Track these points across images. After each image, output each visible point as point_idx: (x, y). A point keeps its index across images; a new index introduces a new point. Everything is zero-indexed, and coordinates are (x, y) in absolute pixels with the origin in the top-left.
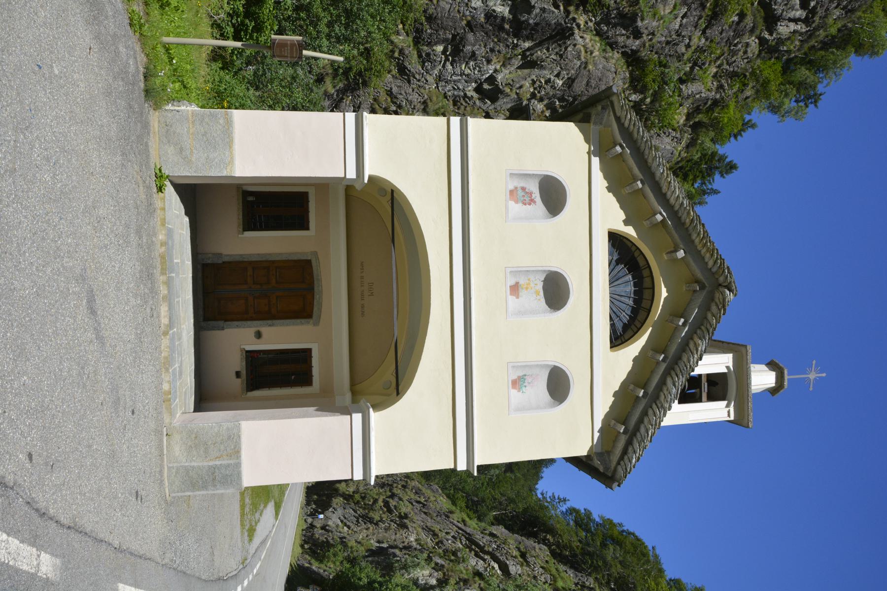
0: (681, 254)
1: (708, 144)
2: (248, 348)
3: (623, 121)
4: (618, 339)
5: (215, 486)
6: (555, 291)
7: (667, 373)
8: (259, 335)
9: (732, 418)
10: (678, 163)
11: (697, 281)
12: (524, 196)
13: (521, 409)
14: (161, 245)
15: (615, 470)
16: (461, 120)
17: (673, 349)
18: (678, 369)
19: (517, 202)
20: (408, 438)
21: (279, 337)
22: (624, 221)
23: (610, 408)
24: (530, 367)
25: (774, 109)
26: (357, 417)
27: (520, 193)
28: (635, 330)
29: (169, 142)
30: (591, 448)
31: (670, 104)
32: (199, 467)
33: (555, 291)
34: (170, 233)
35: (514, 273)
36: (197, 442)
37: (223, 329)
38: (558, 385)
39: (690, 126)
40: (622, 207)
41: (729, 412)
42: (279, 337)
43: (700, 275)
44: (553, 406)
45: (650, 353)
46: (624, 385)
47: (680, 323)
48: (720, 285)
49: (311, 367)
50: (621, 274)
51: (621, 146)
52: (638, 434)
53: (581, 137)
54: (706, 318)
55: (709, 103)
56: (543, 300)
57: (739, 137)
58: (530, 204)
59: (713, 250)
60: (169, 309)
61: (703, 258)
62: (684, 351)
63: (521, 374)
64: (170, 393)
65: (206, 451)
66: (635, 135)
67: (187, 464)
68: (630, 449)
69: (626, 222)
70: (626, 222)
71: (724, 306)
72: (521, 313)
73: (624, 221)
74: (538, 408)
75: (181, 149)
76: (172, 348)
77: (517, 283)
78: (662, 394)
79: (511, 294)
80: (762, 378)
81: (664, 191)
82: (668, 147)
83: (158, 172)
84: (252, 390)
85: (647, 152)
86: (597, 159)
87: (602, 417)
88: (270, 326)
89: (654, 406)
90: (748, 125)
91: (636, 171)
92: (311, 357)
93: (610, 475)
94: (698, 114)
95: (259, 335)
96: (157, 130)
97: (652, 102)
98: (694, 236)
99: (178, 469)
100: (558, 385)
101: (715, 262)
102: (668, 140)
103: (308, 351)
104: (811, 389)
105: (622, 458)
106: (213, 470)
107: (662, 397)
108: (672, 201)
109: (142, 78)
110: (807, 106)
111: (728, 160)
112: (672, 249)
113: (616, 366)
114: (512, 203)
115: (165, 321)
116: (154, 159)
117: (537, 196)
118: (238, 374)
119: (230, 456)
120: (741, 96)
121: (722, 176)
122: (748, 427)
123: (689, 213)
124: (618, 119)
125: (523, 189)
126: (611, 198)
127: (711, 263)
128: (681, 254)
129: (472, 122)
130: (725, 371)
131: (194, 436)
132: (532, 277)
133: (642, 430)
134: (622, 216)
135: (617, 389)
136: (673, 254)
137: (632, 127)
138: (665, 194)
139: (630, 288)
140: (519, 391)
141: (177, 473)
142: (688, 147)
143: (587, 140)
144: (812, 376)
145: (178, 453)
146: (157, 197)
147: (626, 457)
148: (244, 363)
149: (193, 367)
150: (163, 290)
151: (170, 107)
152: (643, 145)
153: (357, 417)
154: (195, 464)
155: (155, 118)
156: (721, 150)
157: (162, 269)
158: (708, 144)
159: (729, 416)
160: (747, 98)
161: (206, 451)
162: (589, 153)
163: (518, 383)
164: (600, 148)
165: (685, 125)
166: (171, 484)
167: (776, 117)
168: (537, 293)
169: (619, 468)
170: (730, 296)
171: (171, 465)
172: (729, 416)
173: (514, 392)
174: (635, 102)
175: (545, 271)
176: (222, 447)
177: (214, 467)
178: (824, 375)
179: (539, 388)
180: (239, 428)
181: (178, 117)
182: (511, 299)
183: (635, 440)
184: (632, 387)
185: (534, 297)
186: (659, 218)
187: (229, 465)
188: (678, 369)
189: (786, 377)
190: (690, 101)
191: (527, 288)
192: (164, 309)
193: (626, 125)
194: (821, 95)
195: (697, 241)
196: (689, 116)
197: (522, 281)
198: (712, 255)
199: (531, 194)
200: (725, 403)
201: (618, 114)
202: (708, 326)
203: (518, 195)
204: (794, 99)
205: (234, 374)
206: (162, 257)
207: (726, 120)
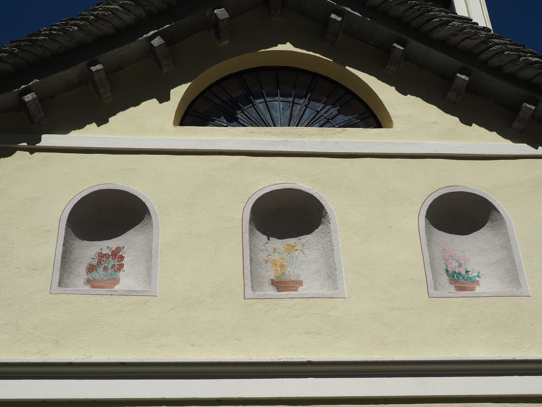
0: (221, 13)
4: (370, 115)
7: (425, 38)
12: (105, 269)
13: (513, 275)
19: (116, 281)
22: (161, 102)
23: (491, 130)
24: (432, 260)
27: (100, 274)
33: (288, 215)
35: (255, 284)
46: (448, 108)
47: (339, 19)
50: (255, 114)
56: (304, 239)
58: (122, 258)
63: (445, 279)
69: (164, 98)
70: (164, 98)
72: (332, 274)
73: (161, 102)
74: (507, 246)
86: (44, 137)
87: (508, 143)
89: (484, 56)
91: (72, 73)
108: (128, 18)
117: (106, 246)
125: (91, 269)
126: (117, 120)
128: (221, 13)
132: (262, 256)
133: (529, 73)
135: (457, 119)
140: (477, 283)
162: (32, 151)
163: (461, 281)
173: (478, 290)
175: (251, 230)
179: (471, 249)
184: (451, 95)
185: (300, 254)
186: (157, 42)
191: (282, 266)
197: (271, 273)
199: (101, 256)
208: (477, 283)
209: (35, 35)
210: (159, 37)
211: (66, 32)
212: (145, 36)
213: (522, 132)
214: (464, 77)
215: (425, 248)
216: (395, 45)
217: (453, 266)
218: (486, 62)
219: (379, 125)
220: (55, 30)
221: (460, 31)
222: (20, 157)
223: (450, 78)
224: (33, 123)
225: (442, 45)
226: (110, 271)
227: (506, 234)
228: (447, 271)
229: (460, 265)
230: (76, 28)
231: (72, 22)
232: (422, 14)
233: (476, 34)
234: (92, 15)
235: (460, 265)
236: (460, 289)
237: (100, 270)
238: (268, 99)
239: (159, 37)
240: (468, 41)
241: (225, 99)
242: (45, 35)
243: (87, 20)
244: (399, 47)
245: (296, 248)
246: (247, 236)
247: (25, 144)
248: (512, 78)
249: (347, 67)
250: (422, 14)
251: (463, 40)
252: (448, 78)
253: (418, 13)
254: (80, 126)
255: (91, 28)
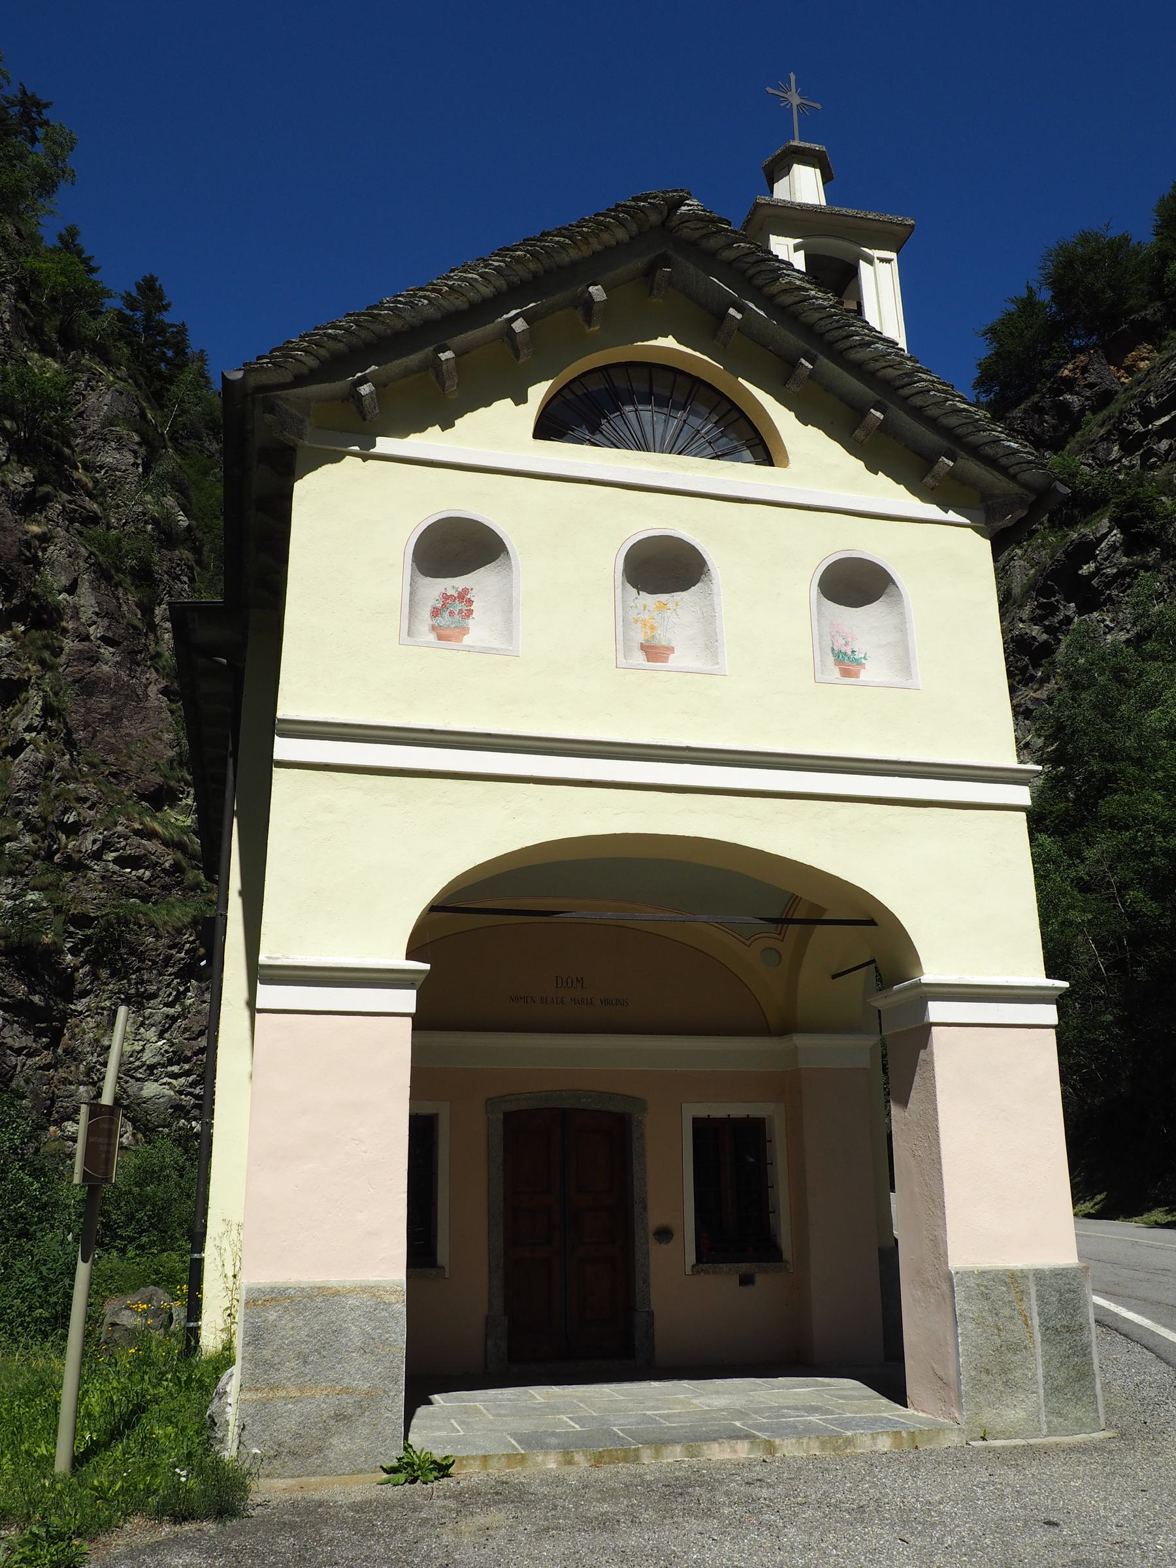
1: (103, 323)
2: (691, 1258)
3: (305, 371)
4: (762, 449)
5: (1081, 1327)
6: (665, 567)
7: (839, 357)
8: (664, 1234)
9: (892, 255)
10: (137, 385)
11: (649, 272)
12: (451, 614)
13: (904, 661)
14: (570, 1462)
15: (1025, 485)
16: (283, 735)
17: (790, 339)
18: (835, 333)
19: (465, 630)
20: (969, 901)
21: (669, 1190)
23: (898, 481)
25: (47, 184)
26: (937, 1011)
27: (444, 620)
28: (734, 415)
29: (320, 1450)
30: (976, 530)
31: (21, 383)
32: (1047, 1363)
33: (665, 567)
34: (535, 1442)
36: (1000, 1371)
37: (651, 1314)
38: (855, 583)
39: (67, 352)
40: (488, 404)
41: (882, 260)
42: (669, 1190)
43: (638, 264)
44: (898, 597)
45: (792, 387)
46: (854, 449)
47: (739, 316)
48: (663, 224)
49: (729, 1120)
51: (362, 381)
52: (960, 431)
53: (327, 471)
54: (730, 263)
55: (24, 306)
56: (678, 596)
57: (93, 264)
58: (470, 602)
59: (599, 223)
60: (715, 1440)
61: (608, 248)
62: (795, 317)
64: (897, 1434)
65: (1014, 1348)
66: (341, 346)
67: (1041, 1392)
68: (988, 450)
69: (520, 399)
70: (520, 399)
71: (713, 221)
72: (710, 643)
74: (902, 628)
75: (340, 1417)
76: (802, 1432)
77: (644, 647)
78: (881, 373)
79: (665, 660)
80: (804, 186)
81: (466, 306)
82: (108, 398)
83: (401, 1477)
84: (779, 1252)
85: (378, 328)
86: (379, 439)
87: (916, 501)
88: (645, 1208)
89: (906, 391)
90: (69, 241)
91: (414, 359)
92: (708, 1120)
93: (1033, 498)
94: (43, 332)
95: (664, 1234)
96: (291, 1482)
97: (12, 417)
98: (564, 258)
99: (1052, 1412)
100: (855, 583)
101: (622, 223)
102: (92, 399)
103: (702, 1127)
104: (818, 106)
105: (1003, 470)
106: (1051, 1333)
107: (890, 372)
108: (486, 291)
109: (188, 1528)
110: (46, 123)
111: (134, 293)
112: (579, 313)
113: (815, 459)
114: (467, 640)
115: (742, 1451)
116: (365, 1487)
118: (746, 1280)
119: (1023, 1294)
120: (15, 243)
121: (166, 308)
122: (912, 227)
123: (518, 260)
124: (300, 380)
125: (436, 613)
127: (621, 234)
129: (286, 709)
130: (802, 253)
131: (984, 1376)
132: (632, 614)
133: (953, 421)
134: (504, 406)
136: (596, 308)
137: (322, 352)
138: (472, 305)
139: (648, 416)
141: (1060, 1414)
142: (107, 362)
143: (337, 458)
144: (795, 100)
145: (1019, 1414)
146: (468, 1475)
147: (1004, 461)
148: (724, 1267)
149: (685, 1384)
150: (675, 1454)
151: (229, 1452)
152: (364, 334)
153: (937, 1011)
154: (1040, 1372)
155: (270, 1489)
156: (113, 304)
157: (625, 1460)
158: (103, 323)
159: (889, 261)
160: (19, 233)
161: (1014, 1348)
162: (365, 458)
163: (847, 664)
164: (354, 430)
165: (64, 362)
166: (1081, 1426)
167: (63, 186)
168: (663, 607)
169: (1023, 477)
170: (692, 205)
171: (1045, 1427)
172: (889, 261)
173: (864, 675)
174: (10, 450)
176: (1006, 1312)
177: (1046, 1329)
178: (793, 77)
180: (966, 1274)
181: (258, 1428)
182: (674, 660)
183: (971, 438)
186: (519, 326)
187: (1041, 1297)
188: (835, 333)
189: (796, 143)
190: (17, 344)
191: (652, 628)
192: (718, 1453)
193: (311, 362)
194: (24, 93)
195: (574, 254)
196: (47, 350)
197: (640, 636)
198: (607, 227)
200: (863, 266)
201: (289, 378)
202: (751, 259)
203: (450, 620)
204: (29, 147)
205: (748, 1289)
206: (598, 1461)
207: (61, 279)
208: (862, 665)
209: (375, 307)
210: (521, 319)
211: (413, 306)
212: (505, 316)
213: (932, 489)
214: (878, 414)
215: (815, 623)
216: (803, 361)
217: (840, 644)
218: (906, 398)
219: (768, 461)
220: (400, 302)
221: (883, 356)
222: (350, 463)
223: (863, 413)
224: (365, 420)
225: (859, 369)
226: (457, 617)
227: (902, 614)
228: (833, 649)
229: (847, 644)
230: (426, 302)
231: (421, 293)
232: (840, 327)
233: (901, 363)
234: (446, 285)
235: (847, 644)
236: (846, 673)
237: (446, 615)
238: (640, 408)
239: (521, 319)
240: (890, 369)
241: (579, 393)
242: (389, 309)
243: (439, 291)
244: (807, 364)
245: (669, 606)
246: (619, 591)
247: (357, 448)
248: (933, 423)
249: (740, 379)
250: (840, 327)
251: (883, 368)
252: (859, 412)
253: (837, 325)
254: (420, 427)
255: (442, 302)
